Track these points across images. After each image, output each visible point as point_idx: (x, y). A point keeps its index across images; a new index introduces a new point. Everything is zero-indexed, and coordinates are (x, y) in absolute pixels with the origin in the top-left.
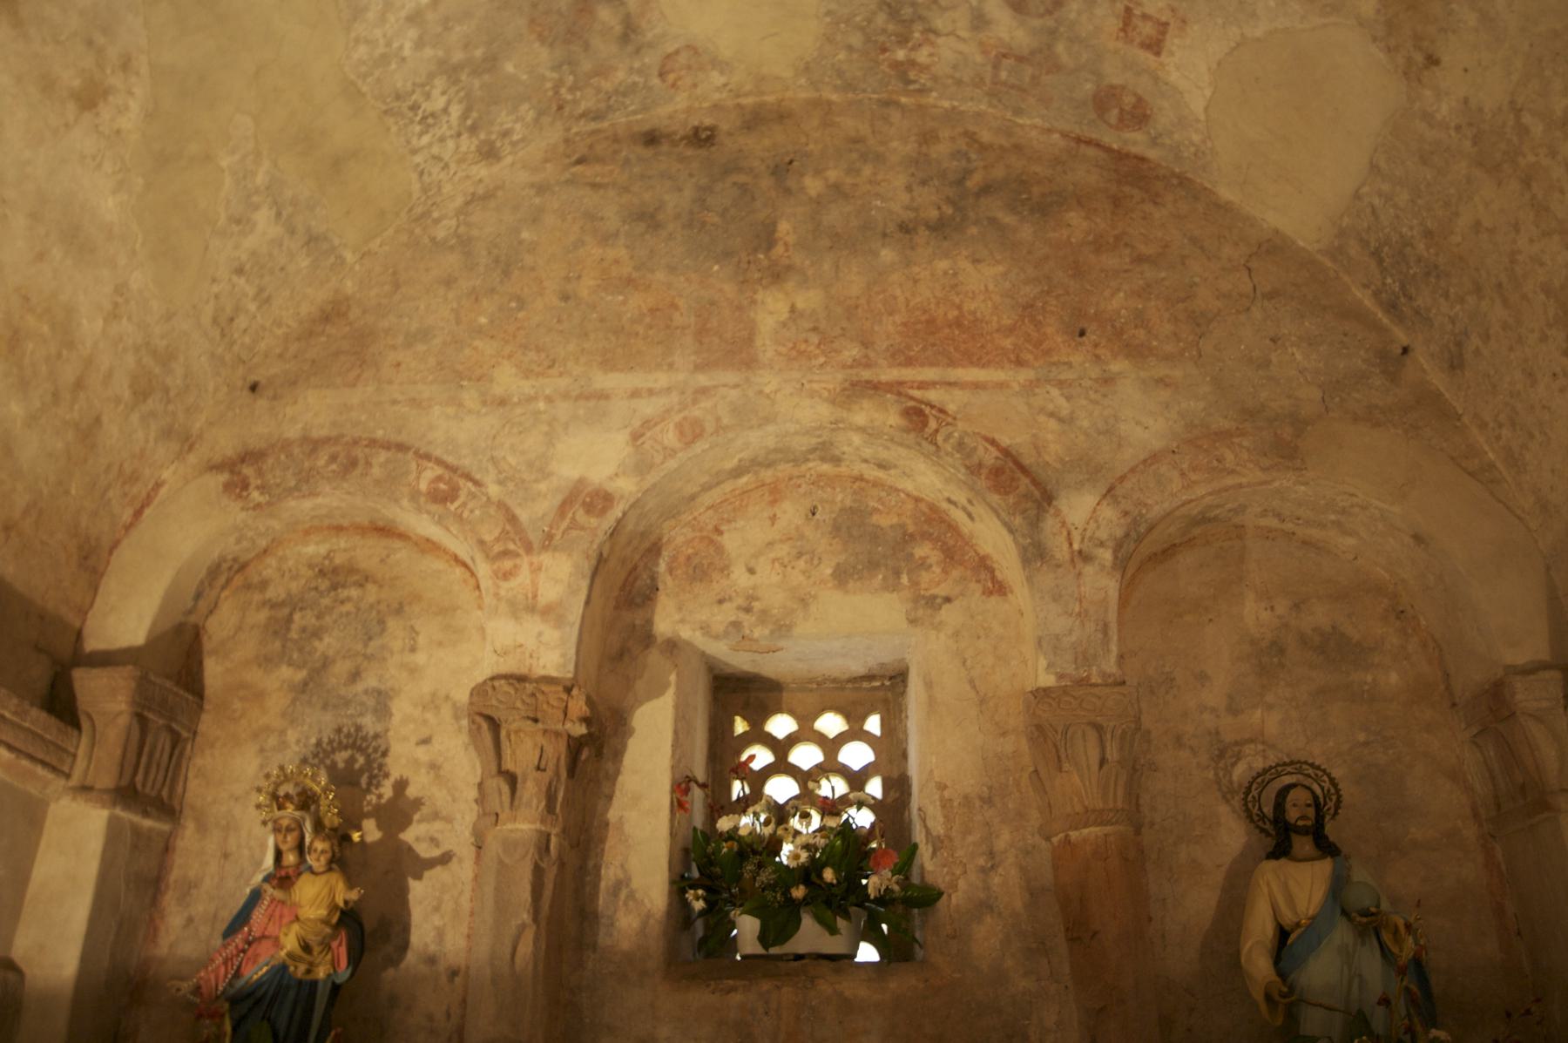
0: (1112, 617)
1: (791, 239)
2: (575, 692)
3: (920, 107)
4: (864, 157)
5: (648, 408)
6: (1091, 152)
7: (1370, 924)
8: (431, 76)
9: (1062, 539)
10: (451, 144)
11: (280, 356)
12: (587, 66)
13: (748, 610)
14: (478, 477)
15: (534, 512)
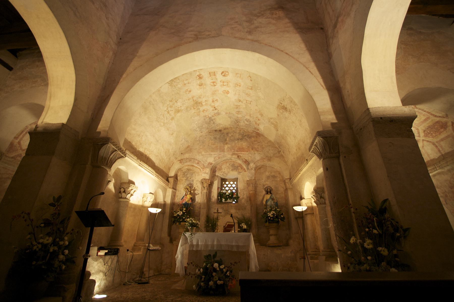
1: (228, 140)
4: (235, 133)
5: (215, 156)
6: (255, 132)
7: (273, 199)
12: (210, 125)
13: (224, 173)
15: (206, 165)
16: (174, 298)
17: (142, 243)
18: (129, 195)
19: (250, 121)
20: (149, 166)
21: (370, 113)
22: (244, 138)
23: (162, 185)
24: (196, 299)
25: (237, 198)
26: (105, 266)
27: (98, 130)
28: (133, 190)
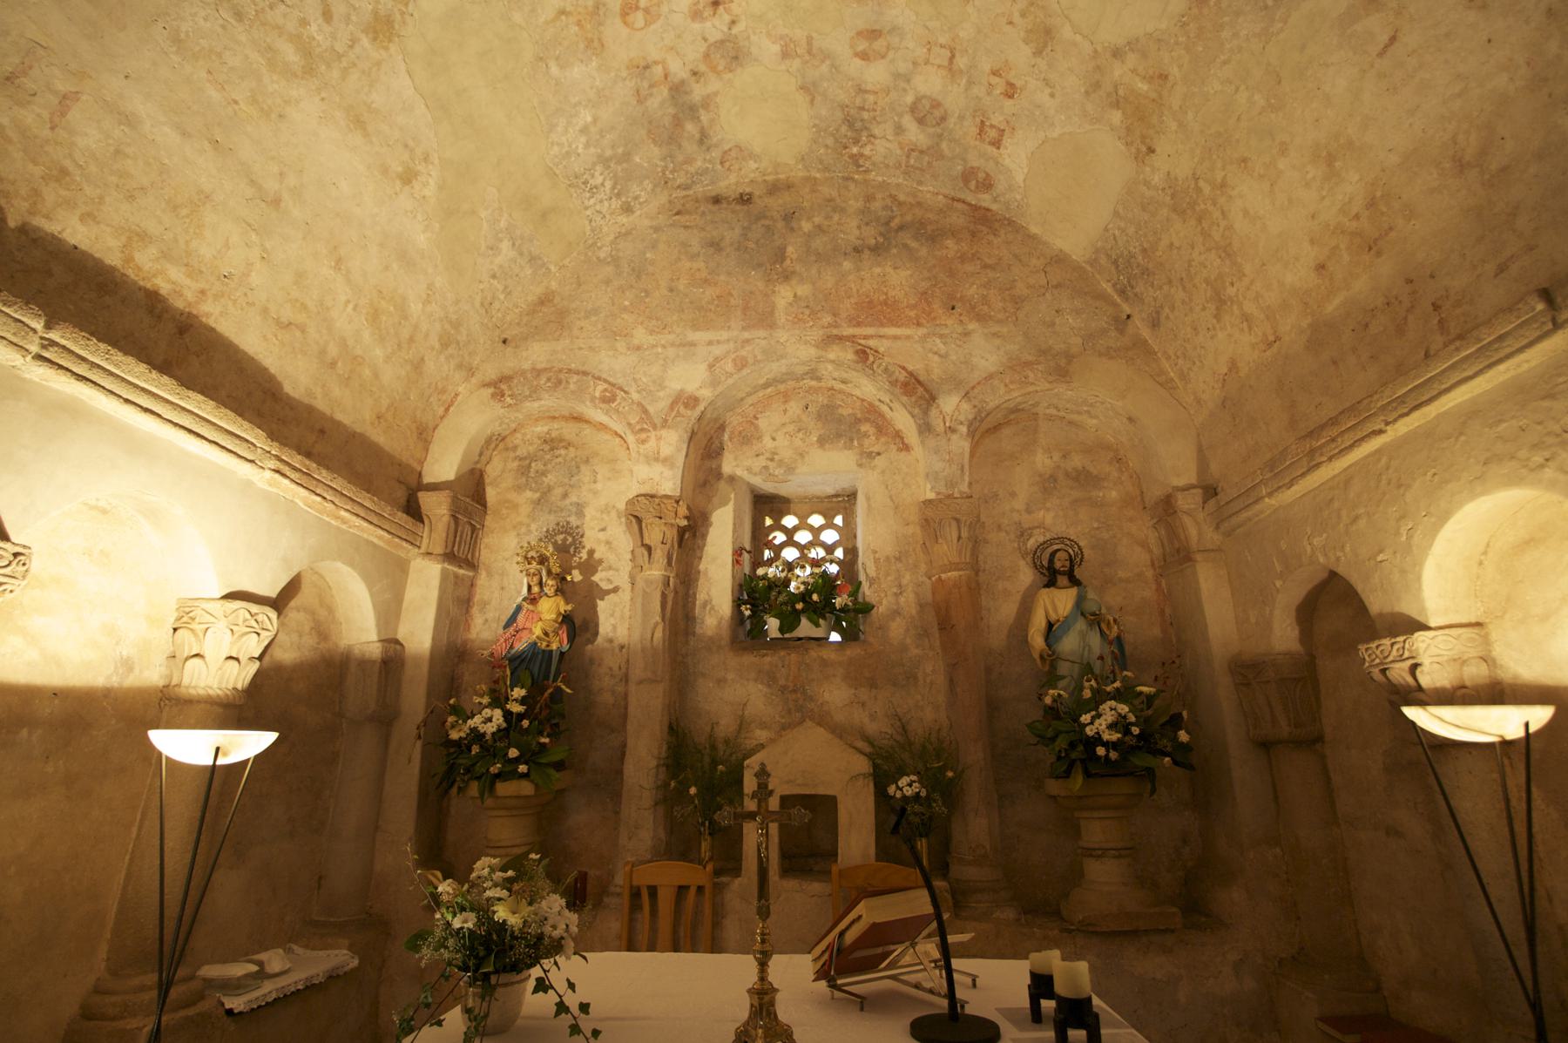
1: (794, 256)
2: (681, 503)
4: (834, 210)
5: (717, 351)
6: (960, 206)
8: (594, 164)
9: (940, 421)
10: (606, 204)
11: (518, 324)
12: (680, 158)
13: (772, 460)
15: (657, 408)
25: (854, 619)
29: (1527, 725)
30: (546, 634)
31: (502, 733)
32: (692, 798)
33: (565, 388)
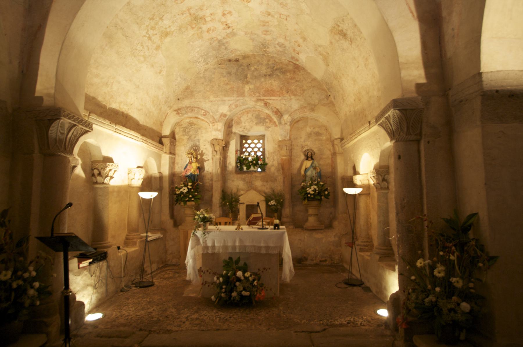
0: (289, 132)
1: (250, 77)
2: (223, 141)
3: (268, 55)
4: (260, 64)
5: (231, 102)
6: (291, 63)
7: (315, 168)
8: (200, 57)
9: (283, 121)
10: (202, 64)
11: (181, 95)
12: (220, 52)
13: (244, 128)
14: (209, 112)
15: (217, 117)
16: (188, 314)
17: (137, 235)
18: (108, 178)
19: (285, 47)
20: (131, 130)
21: (482, 81)
22: (274, 74)
23: (154, 151)
24: (217, 314)
25: (263, 166)
26: (92, 278)
27: (37, 94)
28: (112, 171)
29: (356, 192)
30: (194, 171)
31: (187, 192)
32: (227, 205)
33: (194, 112)
